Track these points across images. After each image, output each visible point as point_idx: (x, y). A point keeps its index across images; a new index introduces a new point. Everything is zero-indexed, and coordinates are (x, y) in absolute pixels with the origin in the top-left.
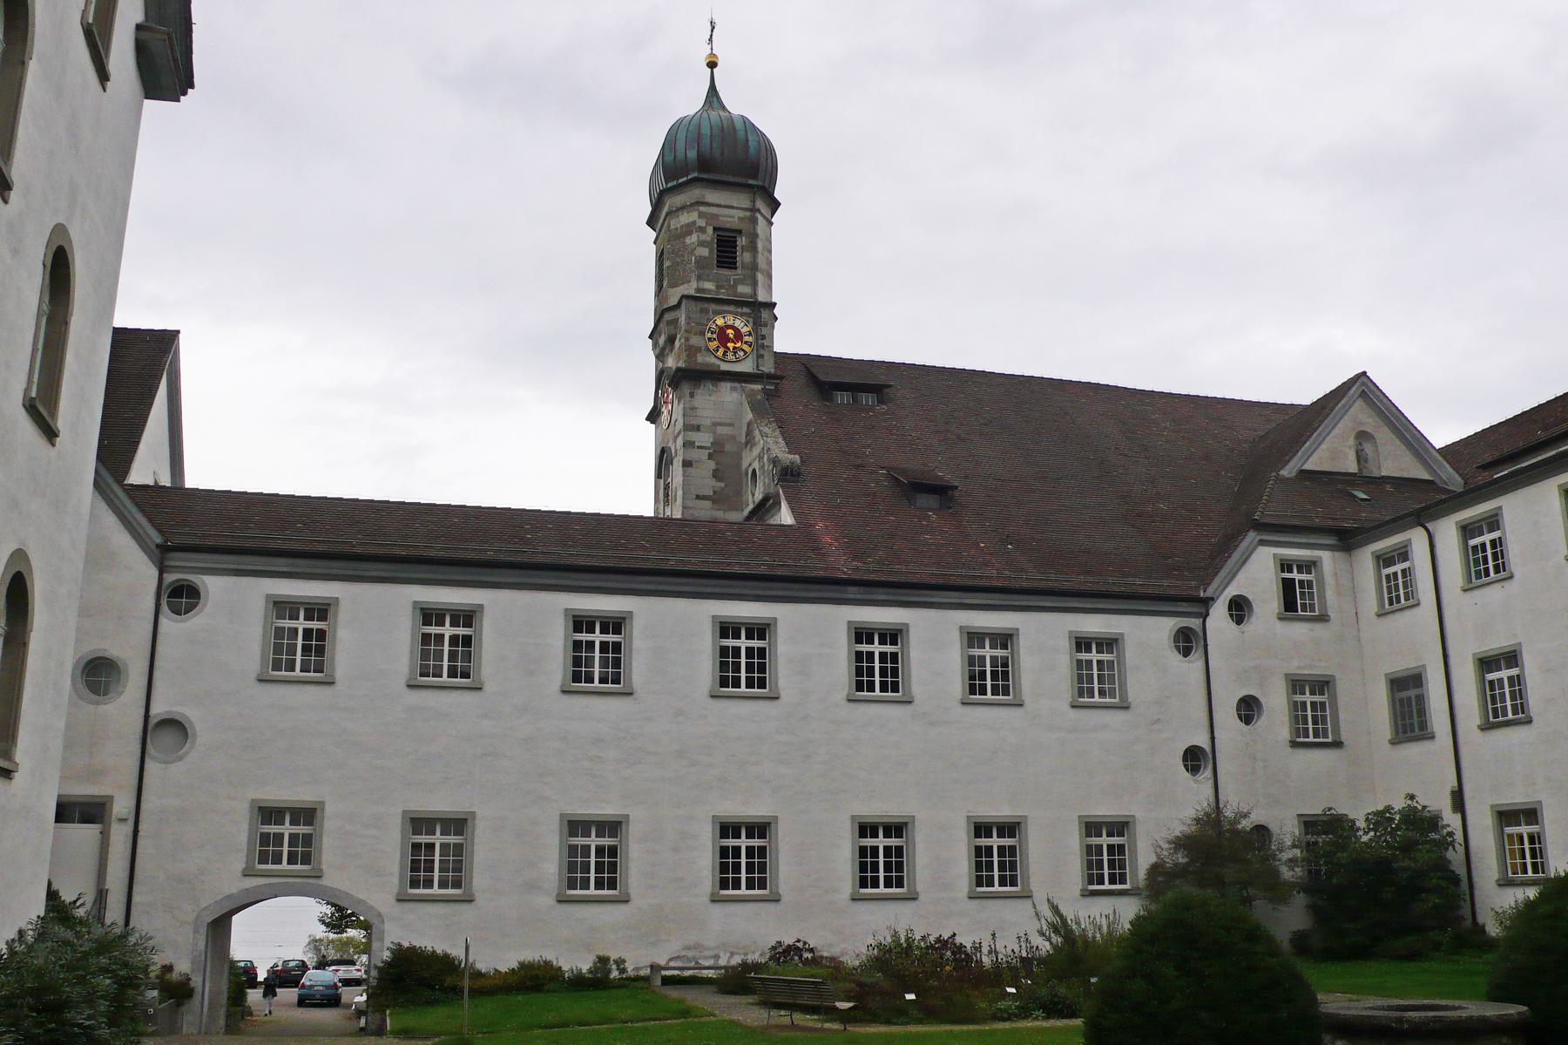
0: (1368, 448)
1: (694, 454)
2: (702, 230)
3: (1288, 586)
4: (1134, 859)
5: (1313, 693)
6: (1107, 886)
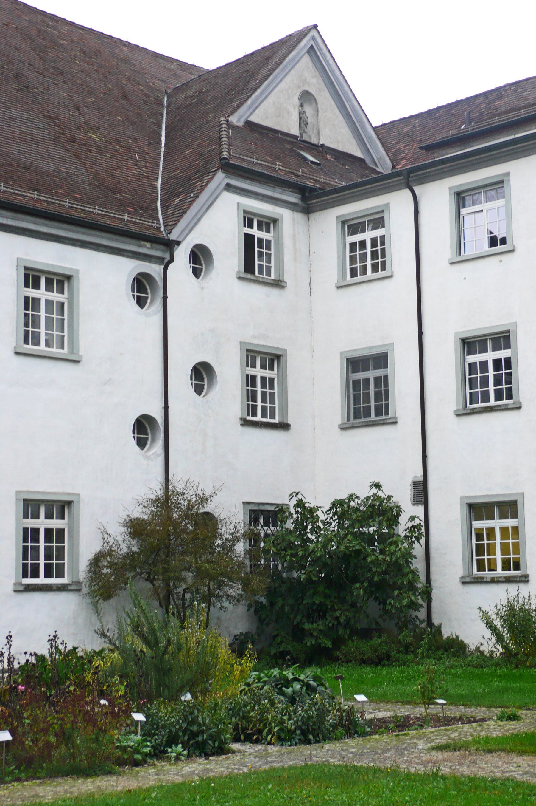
0: (309, 110)
3: (249, 239)
4: (75, 546)
5: (263, 367)
6: (42, 580)
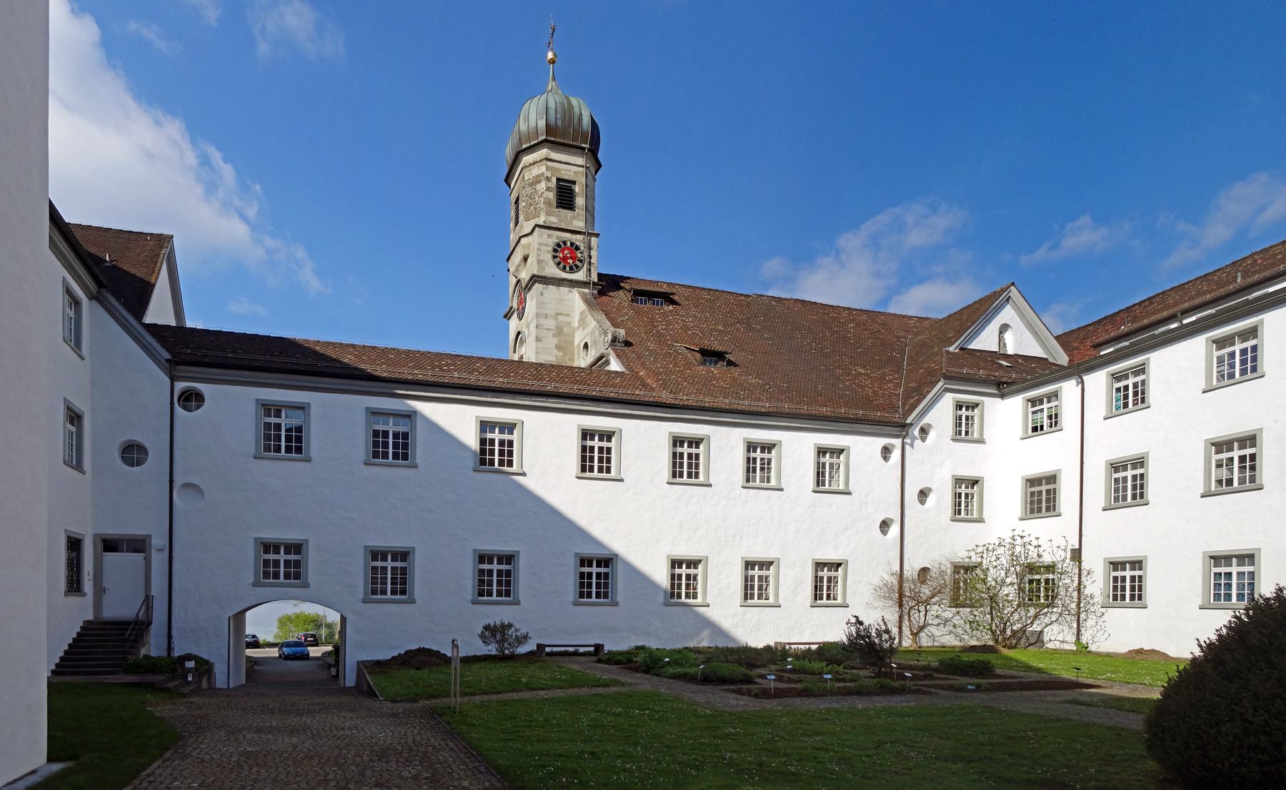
1: (543, 333)
2: (548, 179)
